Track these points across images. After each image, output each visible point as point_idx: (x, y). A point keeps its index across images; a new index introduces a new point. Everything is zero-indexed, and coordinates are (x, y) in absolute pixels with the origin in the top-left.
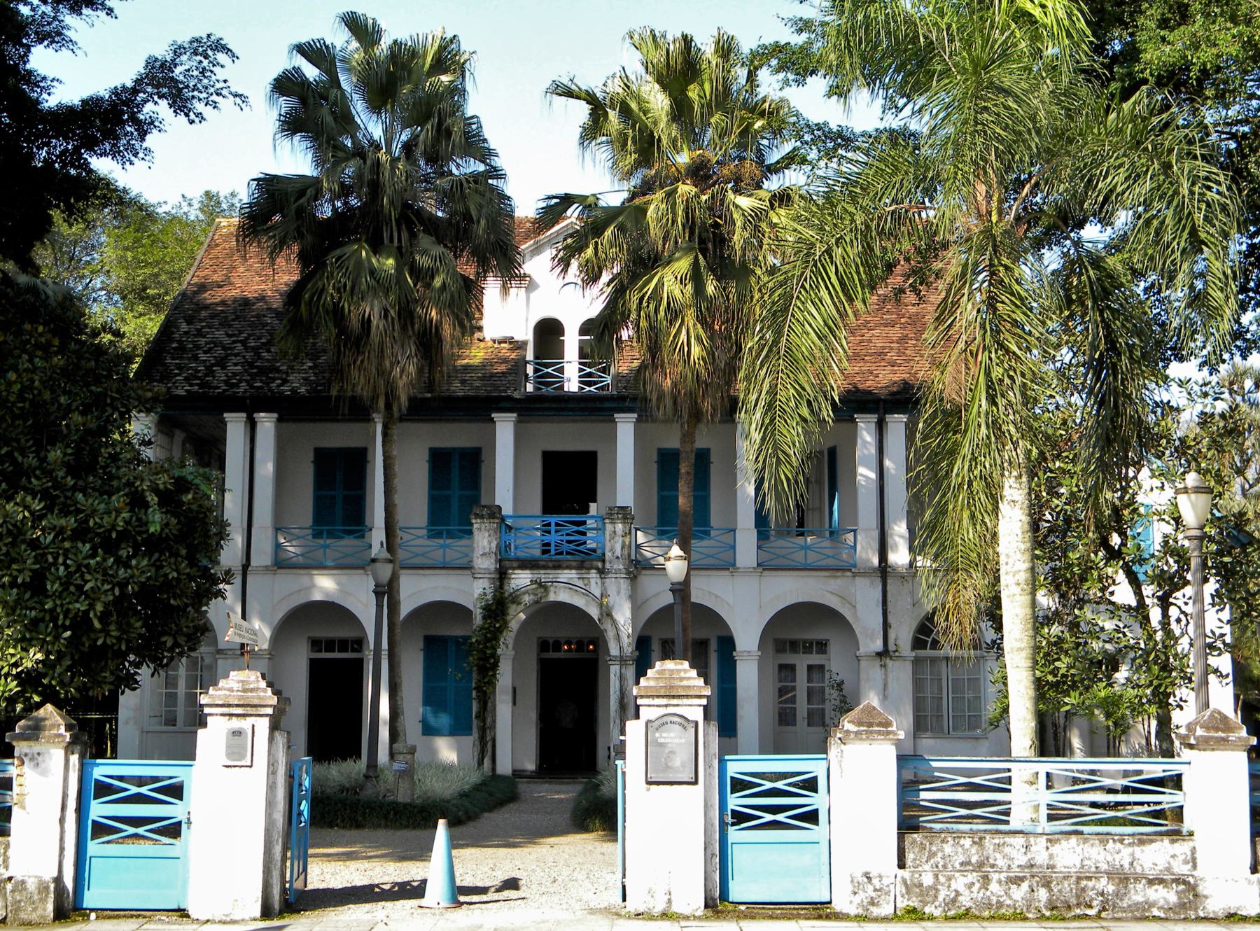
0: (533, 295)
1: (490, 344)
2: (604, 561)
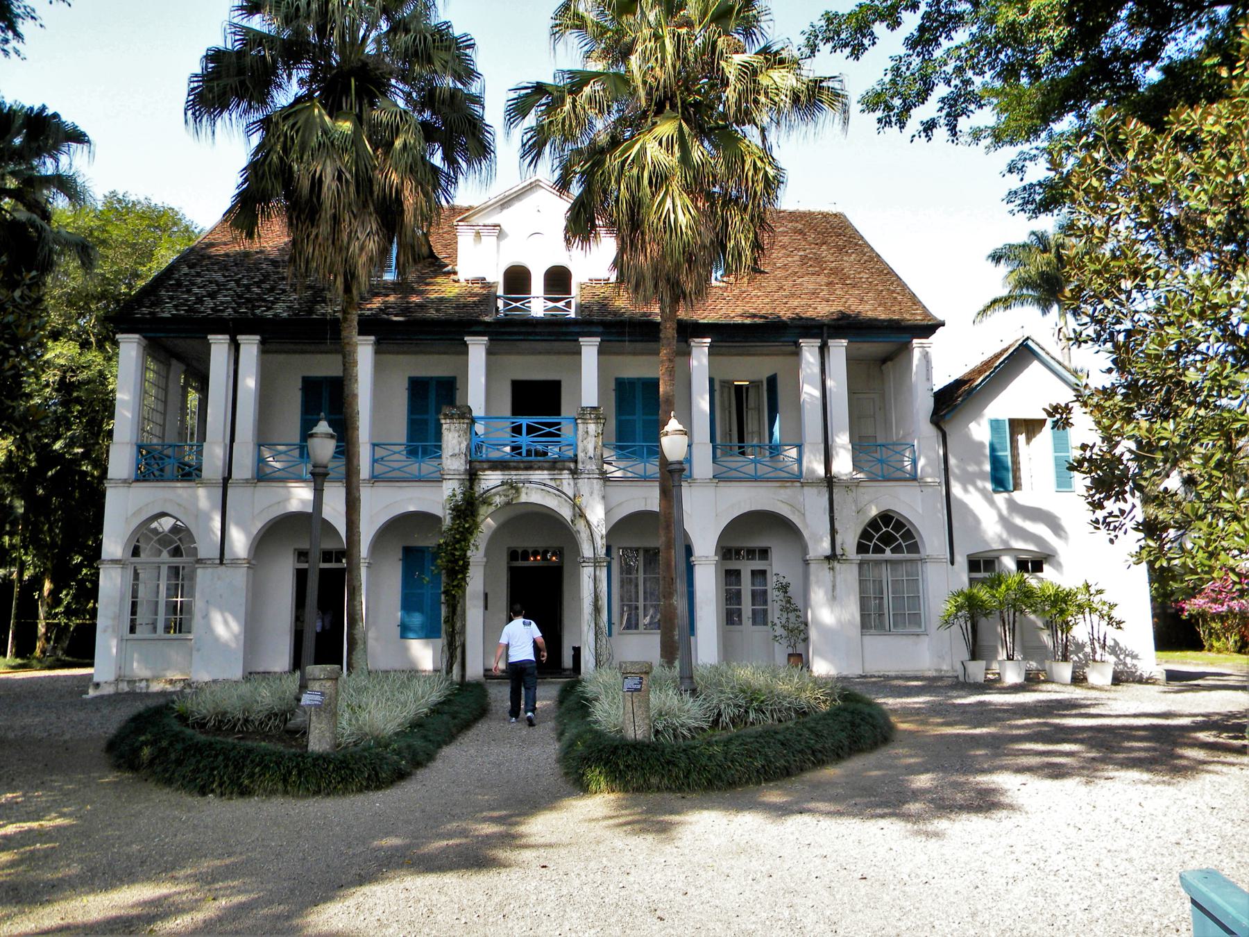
0: (503, 243)
1: (465, 284)
2: (576, 462)
